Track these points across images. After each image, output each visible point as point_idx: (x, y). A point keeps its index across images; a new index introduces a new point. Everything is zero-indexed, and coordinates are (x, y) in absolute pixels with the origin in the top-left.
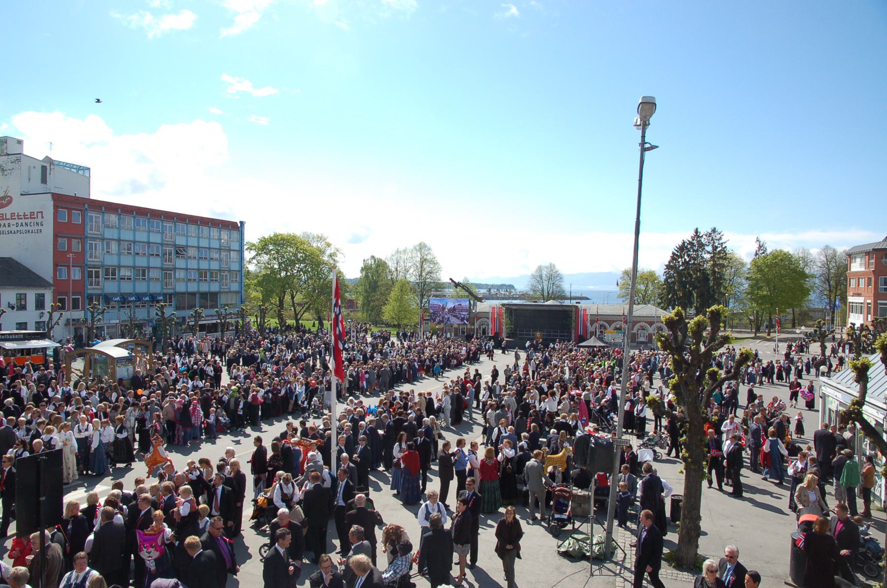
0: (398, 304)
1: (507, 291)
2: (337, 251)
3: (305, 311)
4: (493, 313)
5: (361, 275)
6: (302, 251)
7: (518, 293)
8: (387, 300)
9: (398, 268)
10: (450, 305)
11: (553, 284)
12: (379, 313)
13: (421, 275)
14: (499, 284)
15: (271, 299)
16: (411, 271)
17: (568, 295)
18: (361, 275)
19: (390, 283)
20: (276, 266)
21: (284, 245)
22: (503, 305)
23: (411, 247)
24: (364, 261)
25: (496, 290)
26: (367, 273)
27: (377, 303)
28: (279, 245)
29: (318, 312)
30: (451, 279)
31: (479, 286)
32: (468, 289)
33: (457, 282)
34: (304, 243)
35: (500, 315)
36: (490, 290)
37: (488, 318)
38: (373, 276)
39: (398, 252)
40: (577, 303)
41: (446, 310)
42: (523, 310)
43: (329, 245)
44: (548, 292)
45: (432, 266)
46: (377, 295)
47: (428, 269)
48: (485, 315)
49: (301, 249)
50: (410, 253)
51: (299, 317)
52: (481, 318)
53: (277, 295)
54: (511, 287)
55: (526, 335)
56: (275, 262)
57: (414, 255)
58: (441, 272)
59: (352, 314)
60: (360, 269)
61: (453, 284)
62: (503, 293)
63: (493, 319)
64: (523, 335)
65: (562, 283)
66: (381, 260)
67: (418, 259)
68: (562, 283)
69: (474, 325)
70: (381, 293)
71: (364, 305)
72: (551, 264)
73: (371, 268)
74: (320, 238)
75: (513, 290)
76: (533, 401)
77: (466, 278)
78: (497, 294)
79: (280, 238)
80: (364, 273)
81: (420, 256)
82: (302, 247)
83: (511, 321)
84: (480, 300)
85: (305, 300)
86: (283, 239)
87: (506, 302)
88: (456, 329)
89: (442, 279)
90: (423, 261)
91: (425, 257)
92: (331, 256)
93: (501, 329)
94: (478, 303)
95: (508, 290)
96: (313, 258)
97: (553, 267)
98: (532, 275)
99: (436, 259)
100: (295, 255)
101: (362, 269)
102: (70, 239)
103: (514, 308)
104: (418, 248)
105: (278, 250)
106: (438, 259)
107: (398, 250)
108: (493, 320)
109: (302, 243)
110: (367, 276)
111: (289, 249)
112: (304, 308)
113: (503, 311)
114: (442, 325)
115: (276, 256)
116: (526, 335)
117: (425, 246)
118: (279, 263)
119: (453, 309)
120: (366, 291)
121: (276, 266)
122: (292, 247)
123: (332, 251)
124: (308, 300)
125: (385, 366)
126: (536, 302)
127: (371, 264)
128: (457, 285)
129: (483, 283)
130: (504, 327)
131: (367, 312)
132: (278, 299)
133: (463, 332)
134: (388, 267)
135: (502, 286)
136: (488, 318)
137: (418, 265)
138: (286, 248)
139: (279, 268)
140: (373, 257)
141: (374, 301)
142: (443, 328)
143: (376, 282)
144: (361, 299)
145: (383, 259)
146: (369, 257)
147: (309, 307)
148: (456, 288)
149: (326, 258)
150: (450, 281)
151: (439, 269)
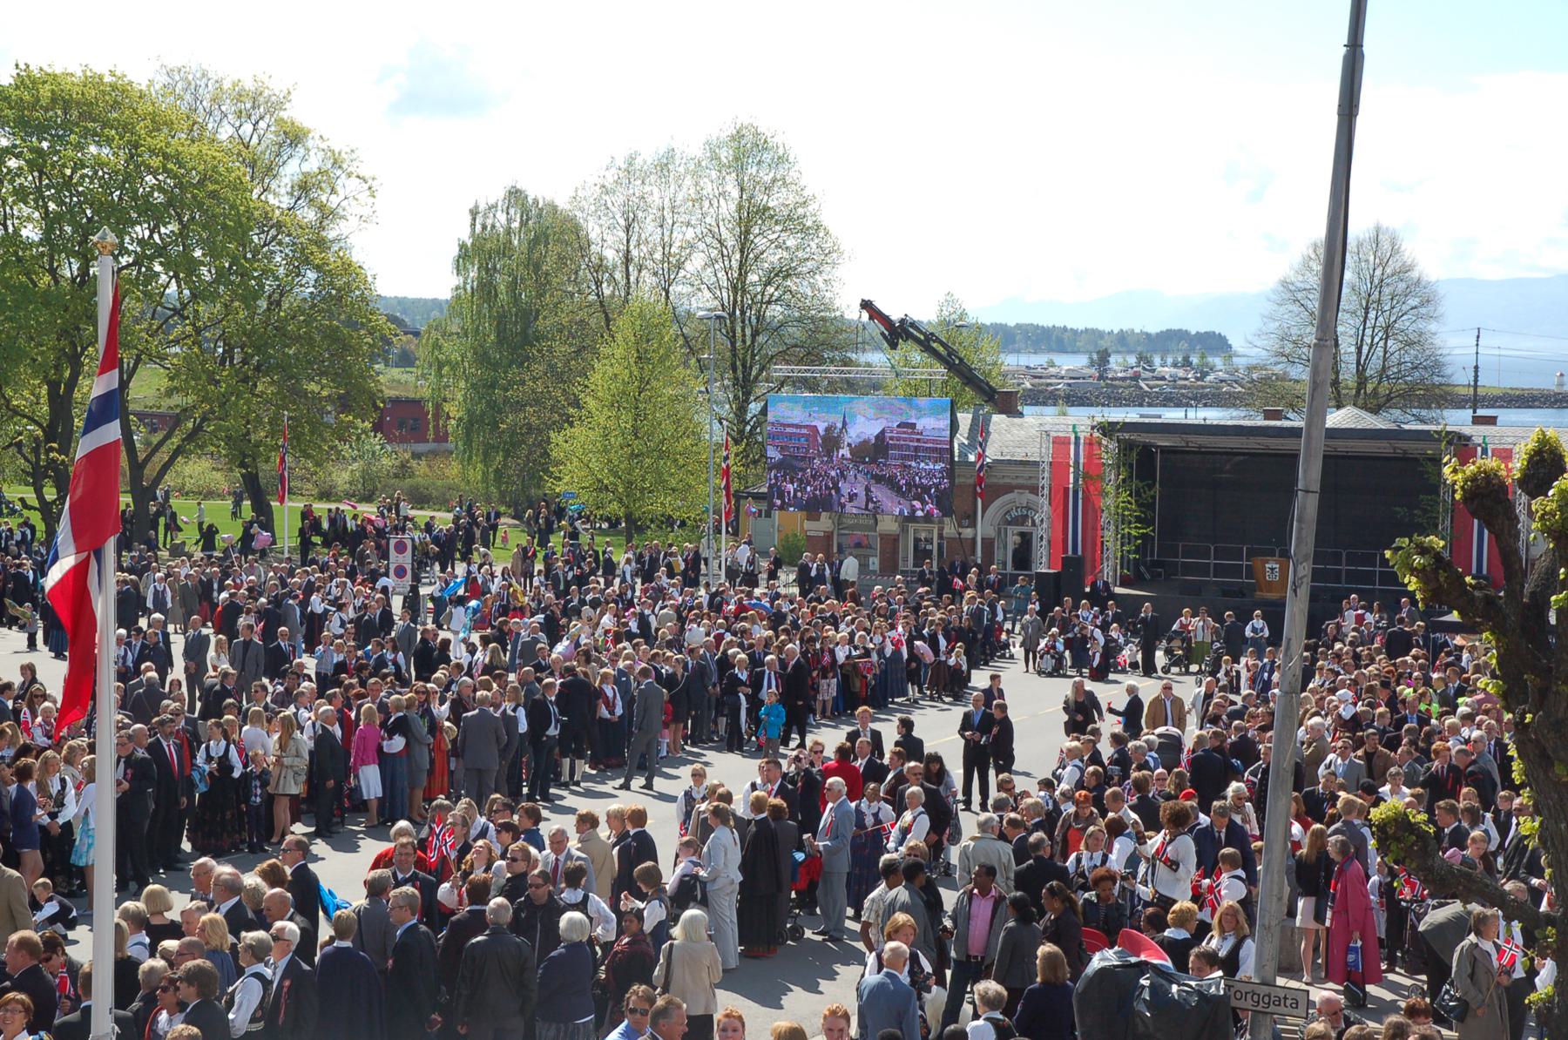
0: (626, 420)
1: (1187, 363)
2: (337, 163)
3: (178, 452)
4: (1058, 467)
5: (456, 281)
6: (156, 162)
7: (1241, 373)
8: (577, 404)
9: (635, 253)
10: (864, 425)
11: (1388, 328)
12: (541, 464)
13: (739, 286)
14: (1154, 328)
15: (9, 392)
16: (696, 263)
17: (1461, 378)
18: (456, 281)
19: (595, 321)
20: (31, 233)
21: (67, 126)
22: (1108, 429)
23: (692, 146)
24: (474, 213)
25: (1132, 360)
26: (488, 270)
27: (530, 415)
28: (41, 130)
29: (243, 454)
30: (867, 305)
31: (1008, 337)
32: (951, 352)
33: (895, 316)
34: (169, 124)
35: (1091, 475)
36: (1103, 357)
37: (1034, 490)
38: (513, 286)
39: (629, 170)
40: (1477, 420)
41: (845, 452)
42: (1202, 453)
43: (294, 137)
44: (1361, 369)
45: (791, 242)
46: (533, 379)
47: (773, 258)
48: (1018, 475)
49: (153, 152)
50: (688, 181)
51: (150, 471)
52: (1009, 489)
53: (38, 369)
54: (1215, 343)
55: (1219, 571)
56: (26, 211)
57: (709, 188)
58: (839, 272)
59: (420, 467)
60: (455, 251)
61: (876, 329)
62: (1167, 371)
63: (1060, 495)
64: (1203, 570)
65: (1433, 327)
66: (554, 208)
67: (728, 208)
68: (1433, 327)
69: (973, 525)
70: (552, 367)
71: (471, 424)
72: (1378, 231)
73: (505, 250)
74: (252, 103)
75: (1218, 362)
76: (1098, 856)
77: (950, 299)
78: (1136, 377)
79: (45, 92)
80: (473, 274)
81: (735, 193)
82: (159, 141)
83: (1143, 505)
84: (1007, 404)
85: (177, 399)
86: (61, 100)
87: (1131, 415)
88: (891, 543)
89: (837, 303)
90: (751, 217)
91: (761, 198)
92: (304, 188)
93: (1094, 542)
94: (998, 419)
95: (1195, 360)
96: (214, 195)
97: (1386, 246)
98: (1285, 284)
99: (812, 208)
100: (130, 178)
101: (465, 256)
102: (1537, 811)
103: (1164, 442)
104: (725, 154)
105: (39, 152)
106: (831, 214)
107: (631, 161)
108: (1060, 495)
109: (158, 123)
110: (486, 289)
111: (93, 149)
112: (175, 441)
113: (1108, 459)
114: (824, 523)
115: (28, 181)
116: (1219, 571)
117: (761, 145)
118: (46, 214)
119: (877, 449)
120: (482, 358)
121: (31, 233)
122: (109, 141)
123: (312, 165)
124: (191, 399)
125: (484, 701)
126: (1277, 415)
127: (509, 231)
128: (898, 333)
129: (1077, 323)
130: (1109, 535)
131: (486, 459)
132: (44, 390)
133: (921, 554)
134: (584, 246)
135: (1169, 339)
136: (1034, 490)
137: (725, 234)
138: (80, 147)
139: (47, 239)
140: (515, 196)
141: (519, 406)
142: (828, 537)
143: (528, 316)
144: (460, 397)
145: (563, 203)
146: (497, 194)
147: (198, 429)
148: (894, 346)
149: (279, 198)
150: (865, 316)
151: (829, 255)
